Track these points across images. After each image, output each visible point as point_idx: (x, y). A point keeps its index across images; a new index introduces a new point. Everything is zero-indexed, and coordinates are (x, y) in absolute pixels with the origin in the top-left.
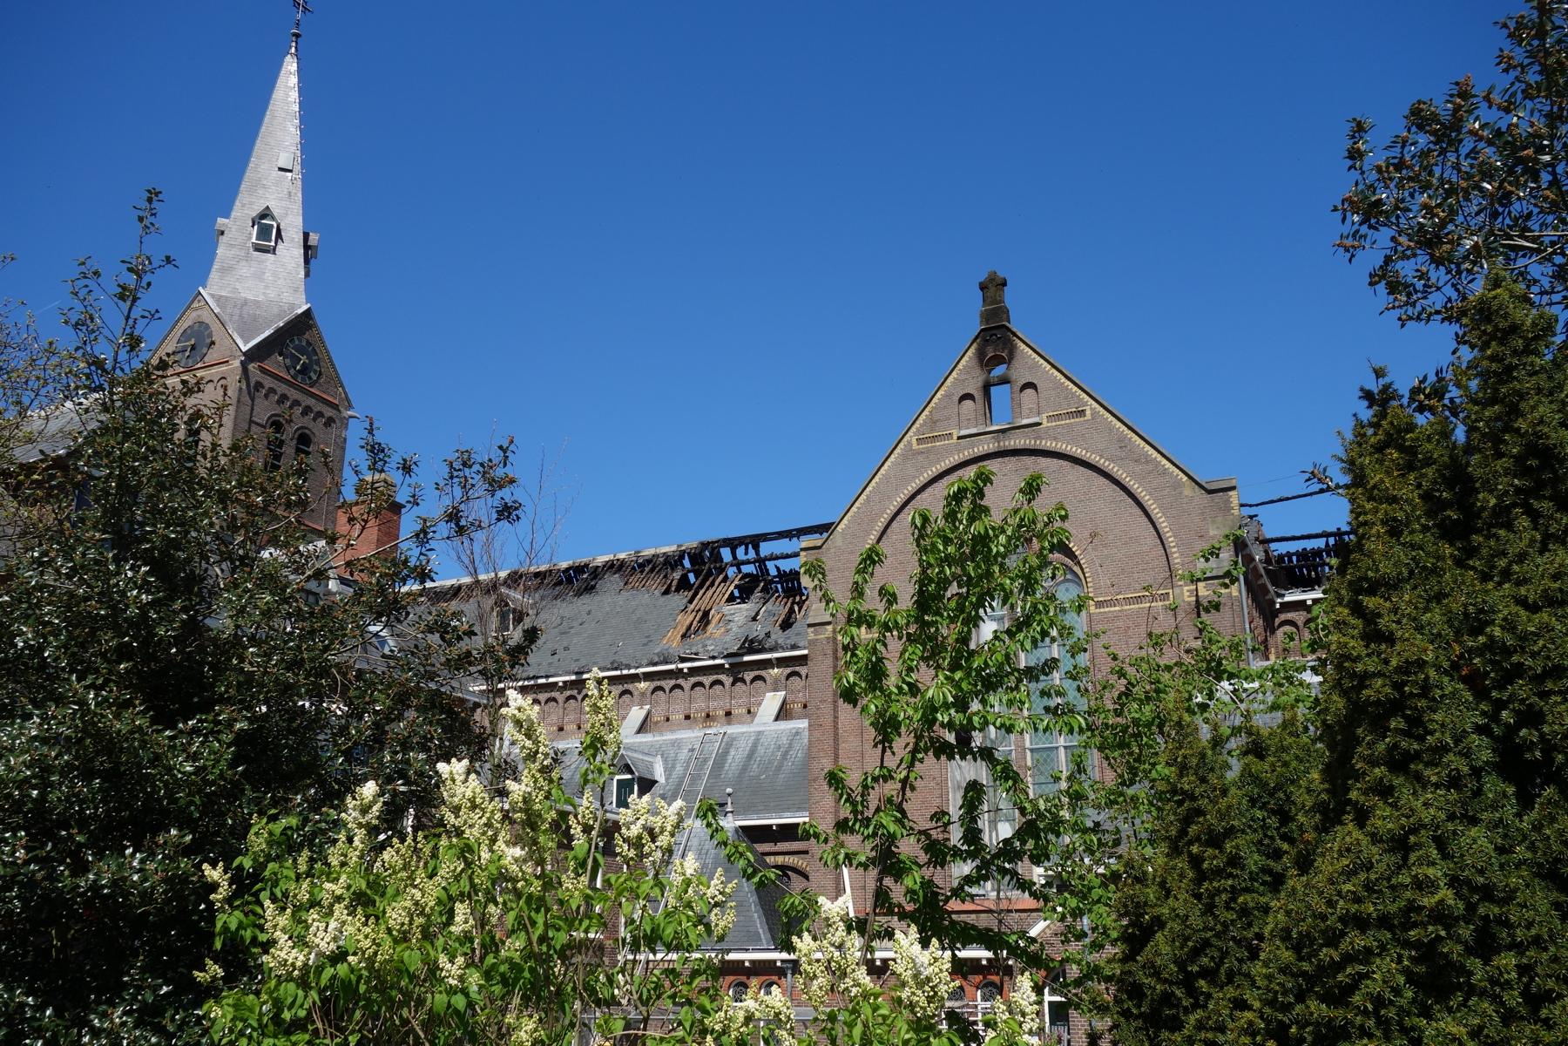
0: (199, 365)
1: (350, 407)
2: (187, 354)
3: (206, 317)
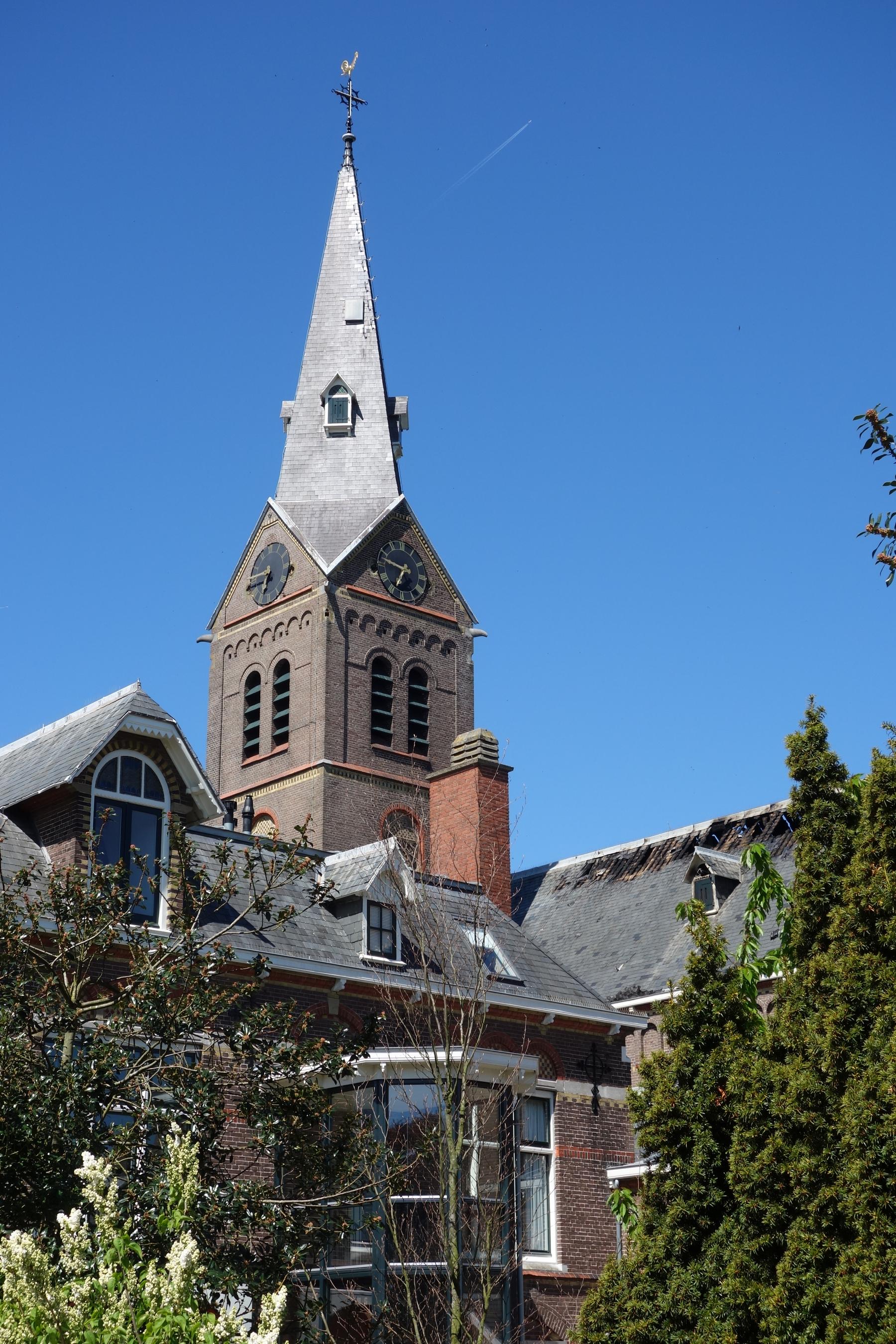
0: (279, 600)
1: (472, 621)
2: (264, 586)
3: (281, 536)
